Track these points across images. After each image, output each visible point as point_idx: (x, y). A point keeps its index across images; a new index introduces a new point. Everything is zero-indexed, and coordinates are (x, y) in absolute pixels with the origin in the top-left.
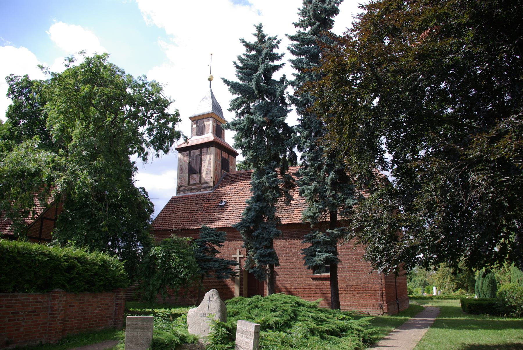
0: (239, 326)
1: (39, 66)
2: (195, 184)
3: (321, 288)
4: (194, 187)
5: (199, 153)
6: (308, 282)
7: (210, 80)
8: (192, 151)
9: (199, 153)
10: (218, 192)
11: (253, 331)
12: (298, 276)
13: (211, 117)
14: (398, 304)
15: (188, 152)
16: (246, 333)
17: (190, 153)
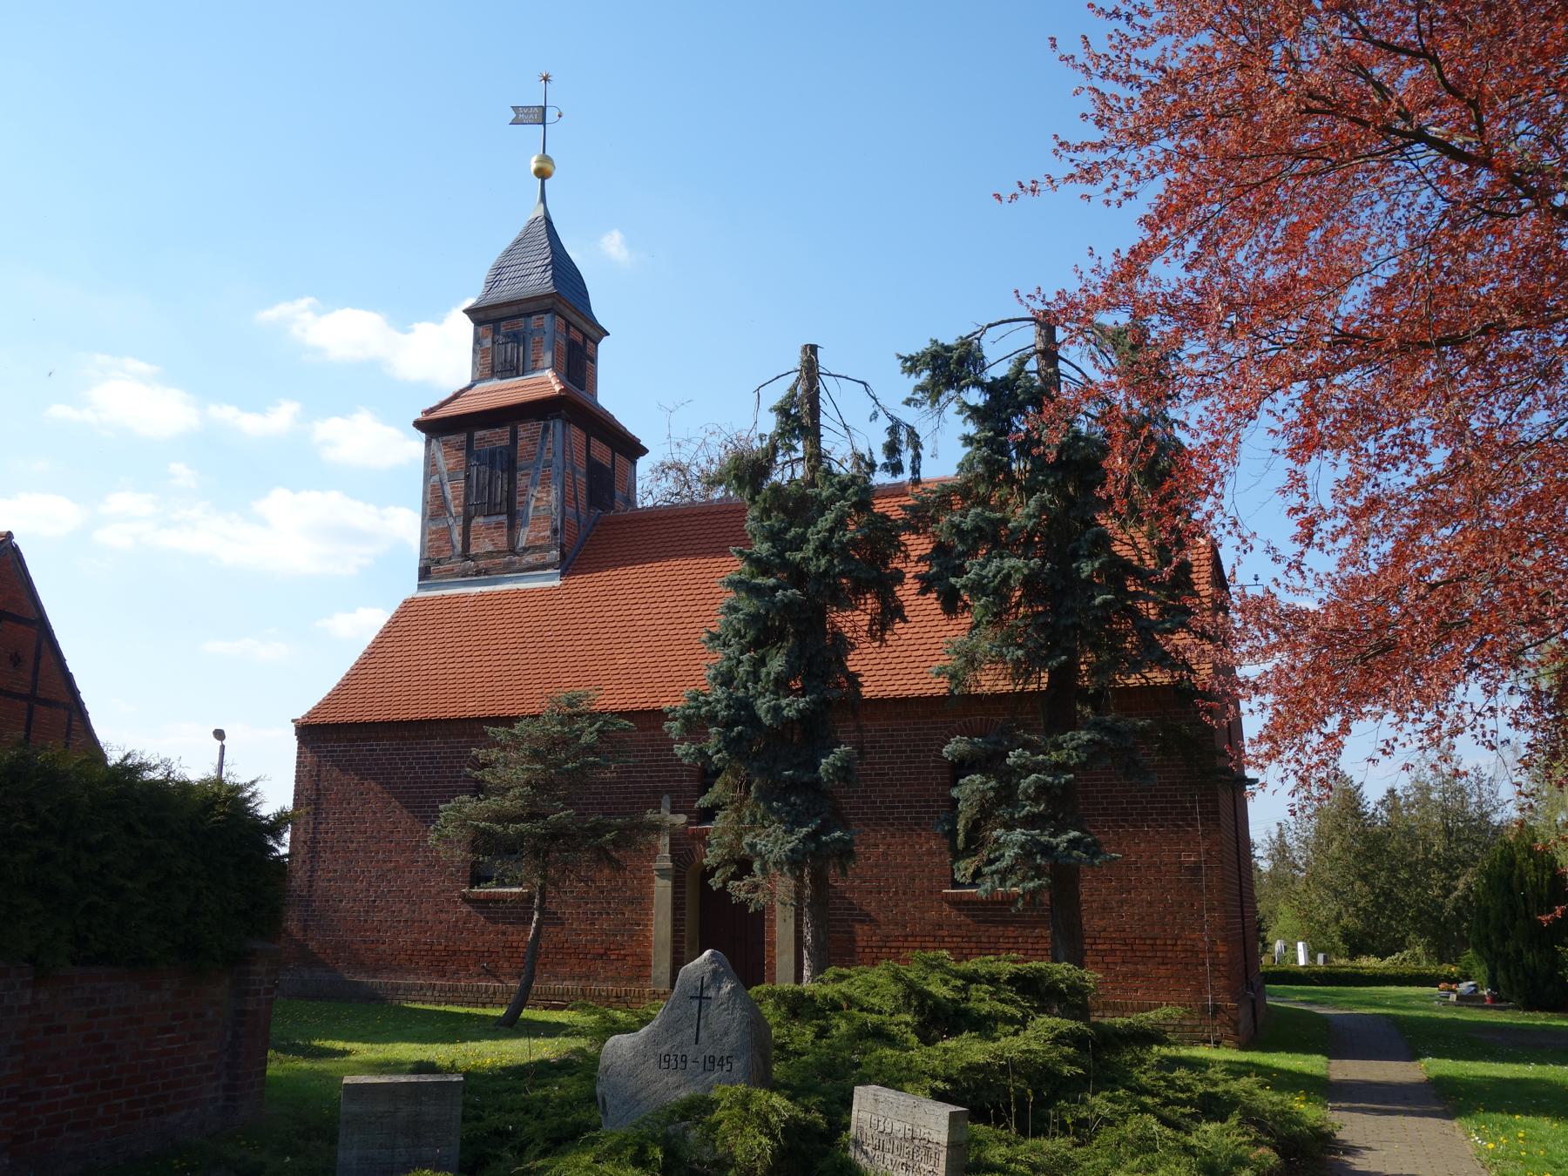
0: (865, 1116)
1: (1020, 183)
2: (489, 555)
3: (984, 939)
4: (482, 564)
5: (506, 442)
6: (932, 915)
7: (542, 174)
8: (478, 434)
9: (506, 442)
10: (1014, 679)
11: (943, 1138)
12: (896, 893)
13: (546, 311)
14: (1253, 1001)
15: (463, 437)
16: (900, 1148)
17: (470, 440)
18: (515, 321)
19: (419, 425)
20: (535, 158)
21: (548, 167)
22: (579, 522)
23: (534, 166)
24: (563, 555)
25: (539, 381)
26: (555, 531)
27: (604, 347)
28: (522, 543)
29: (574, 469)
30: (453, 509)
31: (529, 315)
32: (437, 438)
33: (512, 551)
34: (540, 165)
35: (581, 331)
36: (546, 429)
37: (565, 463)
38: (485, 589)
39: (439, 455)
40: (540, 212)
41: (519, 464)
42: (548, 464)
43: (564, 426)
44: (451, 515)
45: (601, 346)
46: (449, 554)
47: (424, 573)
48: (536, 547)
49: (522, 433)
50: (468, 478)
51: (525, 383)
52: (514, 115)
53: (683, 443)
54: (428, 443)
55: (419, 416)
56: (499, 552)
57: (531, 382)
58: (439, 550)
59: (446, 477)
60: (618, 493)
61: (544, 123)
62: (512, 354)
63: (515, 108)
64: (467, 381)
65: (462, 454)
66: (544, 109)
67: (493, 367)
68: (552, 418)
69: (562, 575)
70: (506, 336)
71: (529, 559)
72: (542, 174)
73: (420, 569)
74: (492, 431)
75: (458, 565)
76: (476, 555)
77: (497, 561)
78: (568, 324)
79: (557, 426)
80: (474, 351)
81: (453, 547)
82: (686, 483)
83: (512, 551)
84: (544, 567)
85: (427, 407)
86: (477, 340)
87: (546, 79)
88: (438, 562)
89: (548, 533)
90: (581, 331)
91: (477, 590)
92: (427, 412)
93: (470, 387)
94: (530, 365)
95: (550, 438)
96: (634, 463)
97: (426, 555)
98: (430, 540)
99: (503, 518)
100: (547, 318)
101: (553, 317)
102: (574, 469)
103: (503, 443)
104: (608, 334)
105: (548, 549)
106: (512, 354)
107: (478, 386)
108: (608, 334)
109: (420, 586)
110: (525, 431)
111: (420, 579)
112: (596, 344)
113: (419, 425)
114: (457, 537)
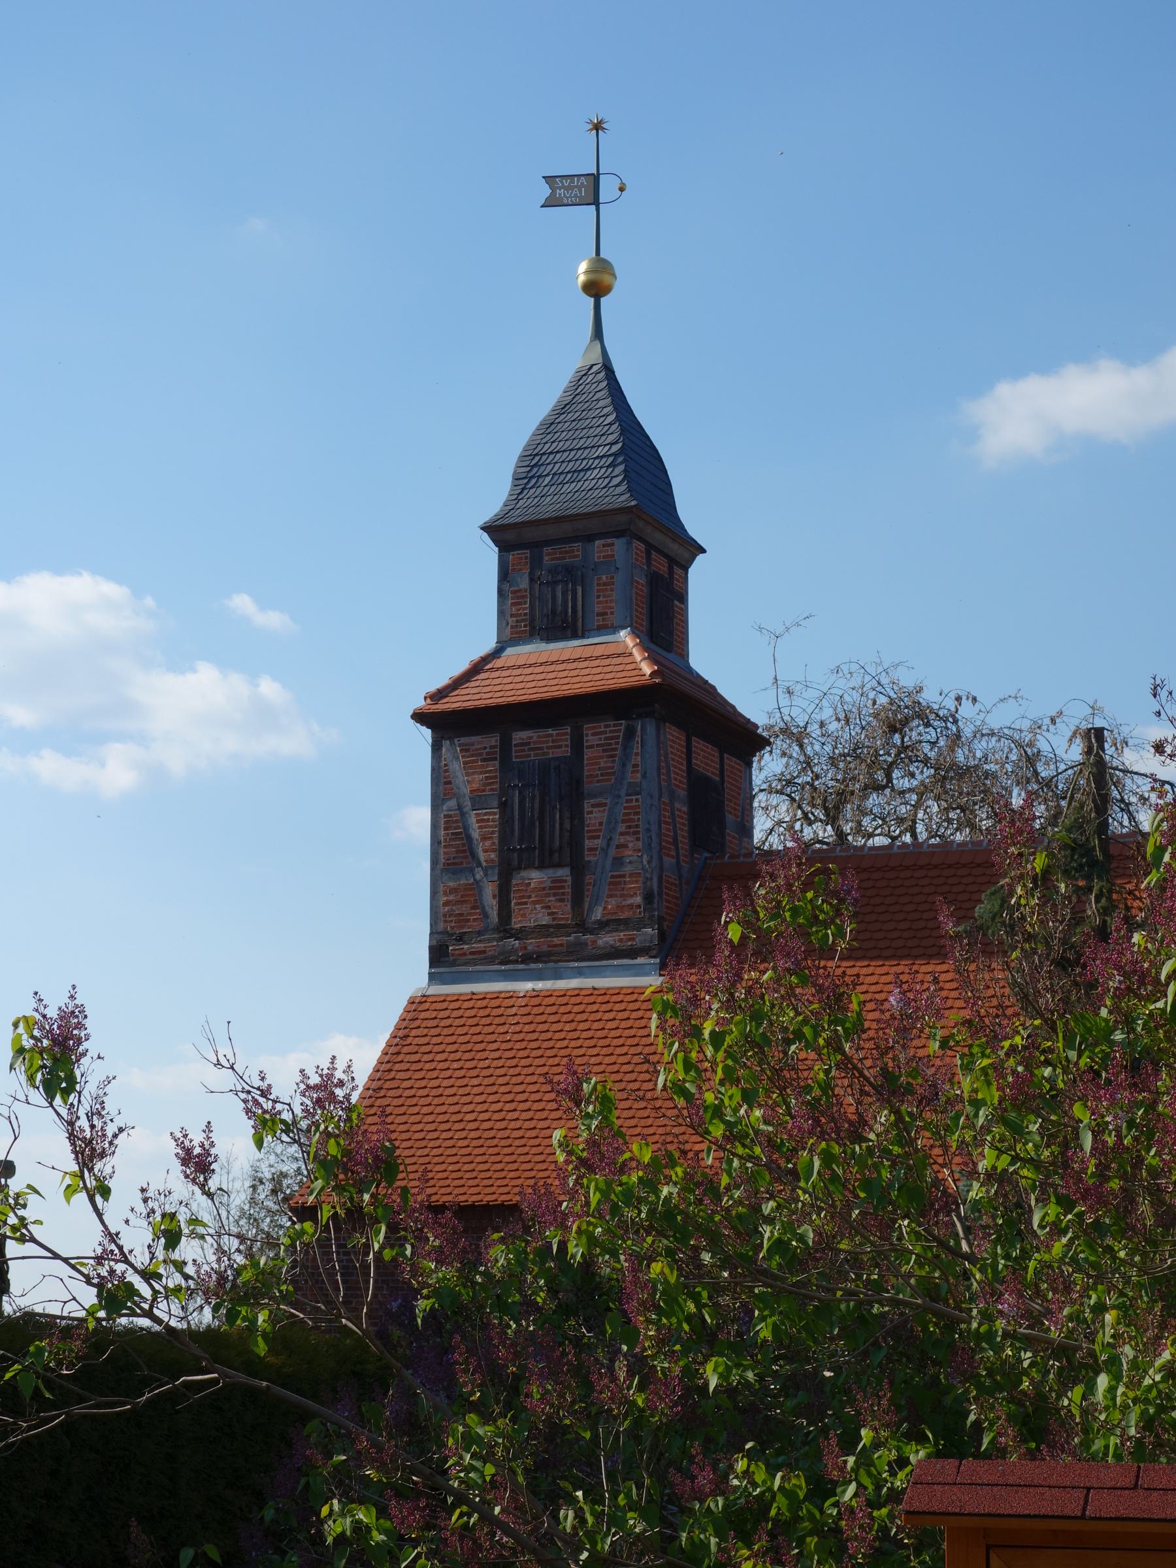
2: (543, 930)
4: (532, 944)
5: (565, 751)
7: (596, 289)
8: (519, 736)
9: (565, 751)
13: (619, 534)
15: (493, 740)
17: (506, 745)
18: (567, 547)
19: (420, 717)
20: (583, 266)
21: (606, 279)
22: (680, 877)
23: (582, 278)
24: (662, 935)
25: (610, 650)
26: (648, 897)
27: (699, 575)
28: (598, 914)
29: (672, 796)
30: (482, 856)
31: (590, 538)
32: (451, 739)
33: (581, 926)
34: (592, 276)
35: (666, 556)
36: (630, 734)
37: (660, 789)
38: (540, 985)
39: (456, 767)
40: (595, 356)
41: (588, 787)
42: (635, 790)
43: (658, 729)
44: (479, 864)
45: (692, 571)
46: (477, 925)
47: (439, 955)
48: (619, 922)
49: (590, 739)
50: (504, 806)
51: (588, 652)
52: (546, 191)
53: (797, 688)
54: (436, 747)
55: (419, 703)
56: (559, 926)
57: (599, 650)
58: (462, 920)
59: (468, 804)
60: (730, 818)
61: (596, 203)
62: (565, 602)
63: (549, 179)
64: (489, 643)
65: (494, 766)
66: (595, 178)
67: (532, 621)
68: (639, 716)
69: (663, 966)
70: (553, 571)
71: (607, 939)
72: (596, 289)
73: (432, 949)
74: (543, 732)
75: (490, 944)
76: (522, 930)
77: (556, 941)
78: (650, 547)
79: (646, 729)
80: (501, 593)
81: (486, 915)
82: (808, 764)
83: (581, 926)
84: (633, 953)
85: (433, 687)
86: (505, 575)
87: (598, 127)
88: (461, 939)
89: (638, 900)
90: (666, 556)
91: (529, 986)
92: (438, 695)
93: (496, 653)
94: (597, 621)
95: (637, 749)
96: (749, 765)
97: (441, 926)
98: (446, 904)
99: (564, 873)
100: (619, 544)
101: (629, 543)
102: (672, 796)
103: (559, 753)
104: (703, 551)
105: (640, 925)
106: (565, 602)
107: (510, 651)
108: (703, 551)
109: (432, 977)
110: (597, 734)
111: (433, 962)
112: (686, 568)
113: (420, 717)
114: (489, 892)
